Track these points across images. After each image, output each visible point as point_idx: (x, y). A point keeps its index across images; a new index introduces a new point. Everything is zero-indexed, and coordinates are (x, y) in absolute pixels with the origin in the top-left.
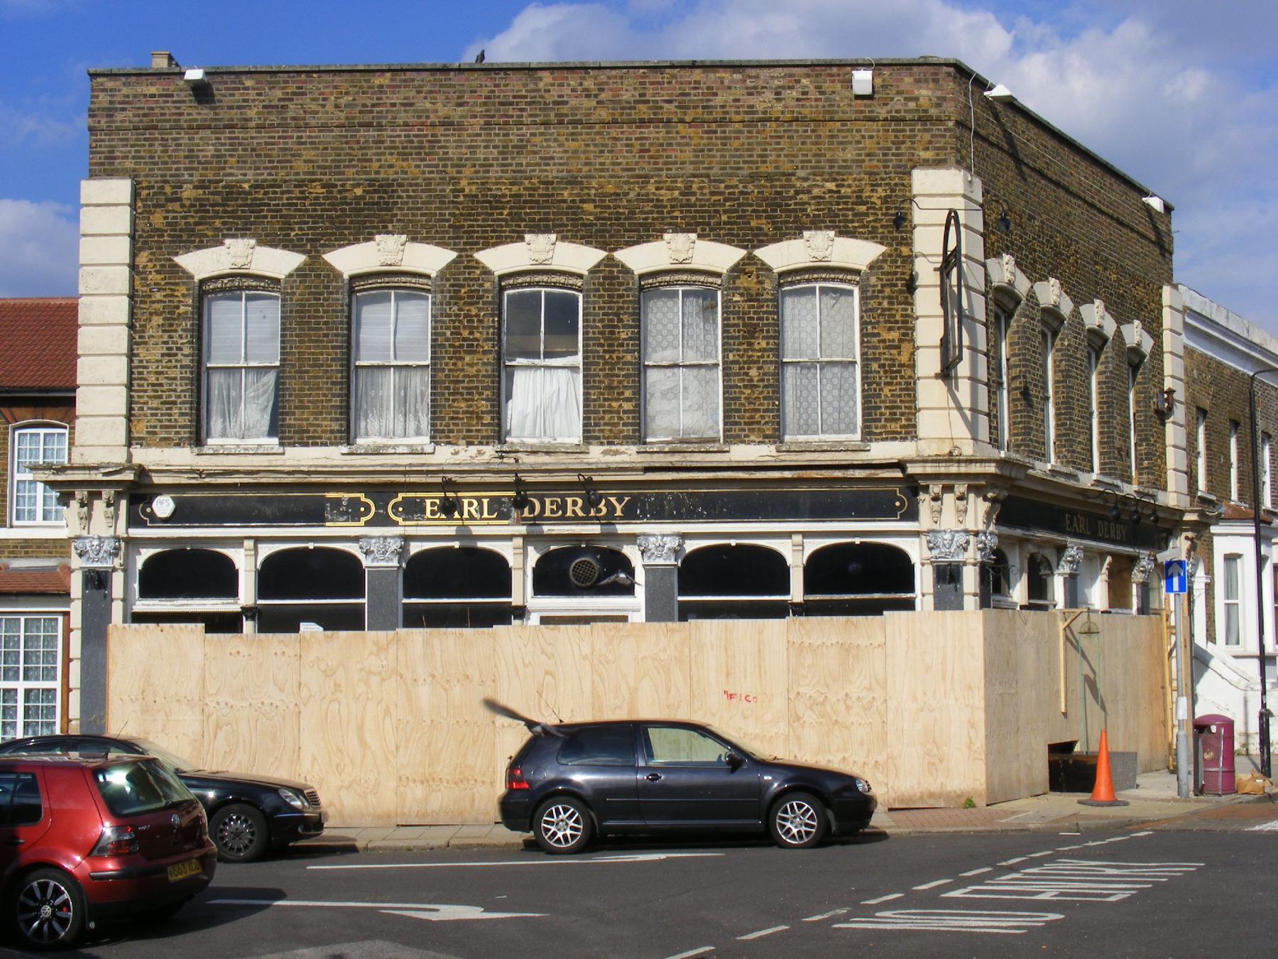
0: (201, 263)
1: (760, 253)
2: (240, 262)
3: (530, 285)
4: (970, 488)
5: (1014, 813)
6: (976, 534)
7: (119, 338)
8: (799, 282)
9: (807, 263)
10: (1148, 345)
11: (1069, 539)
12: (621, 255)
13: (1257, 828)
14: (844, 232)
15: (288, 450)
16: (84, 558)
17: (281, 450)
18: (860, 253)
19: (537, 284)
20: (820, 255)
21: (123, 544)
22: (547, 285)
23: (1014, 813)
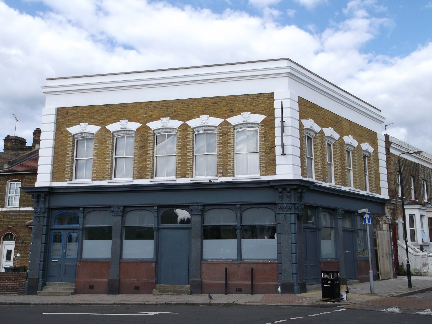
0: (73, 130)
1: (227, 120)
2: (83, 129)
3: (163, 132)
4: (291, 189)
5: (305, 298)
6: (295, 204)
7: (386, 184)
8: (241, 128)
9: (242, 122)
10: (371, 150)
11: (18, 209)
12: (188, 123)
13: (385, 310)
14: (253, 112)
15: (94, 182)
16: (281, 210)
17: (92, 182)
18: (259, 118)
19: (165, 132)
20: (245, 119)
21: (47, 210)
22: (168, 132)
23: (305, 298)
